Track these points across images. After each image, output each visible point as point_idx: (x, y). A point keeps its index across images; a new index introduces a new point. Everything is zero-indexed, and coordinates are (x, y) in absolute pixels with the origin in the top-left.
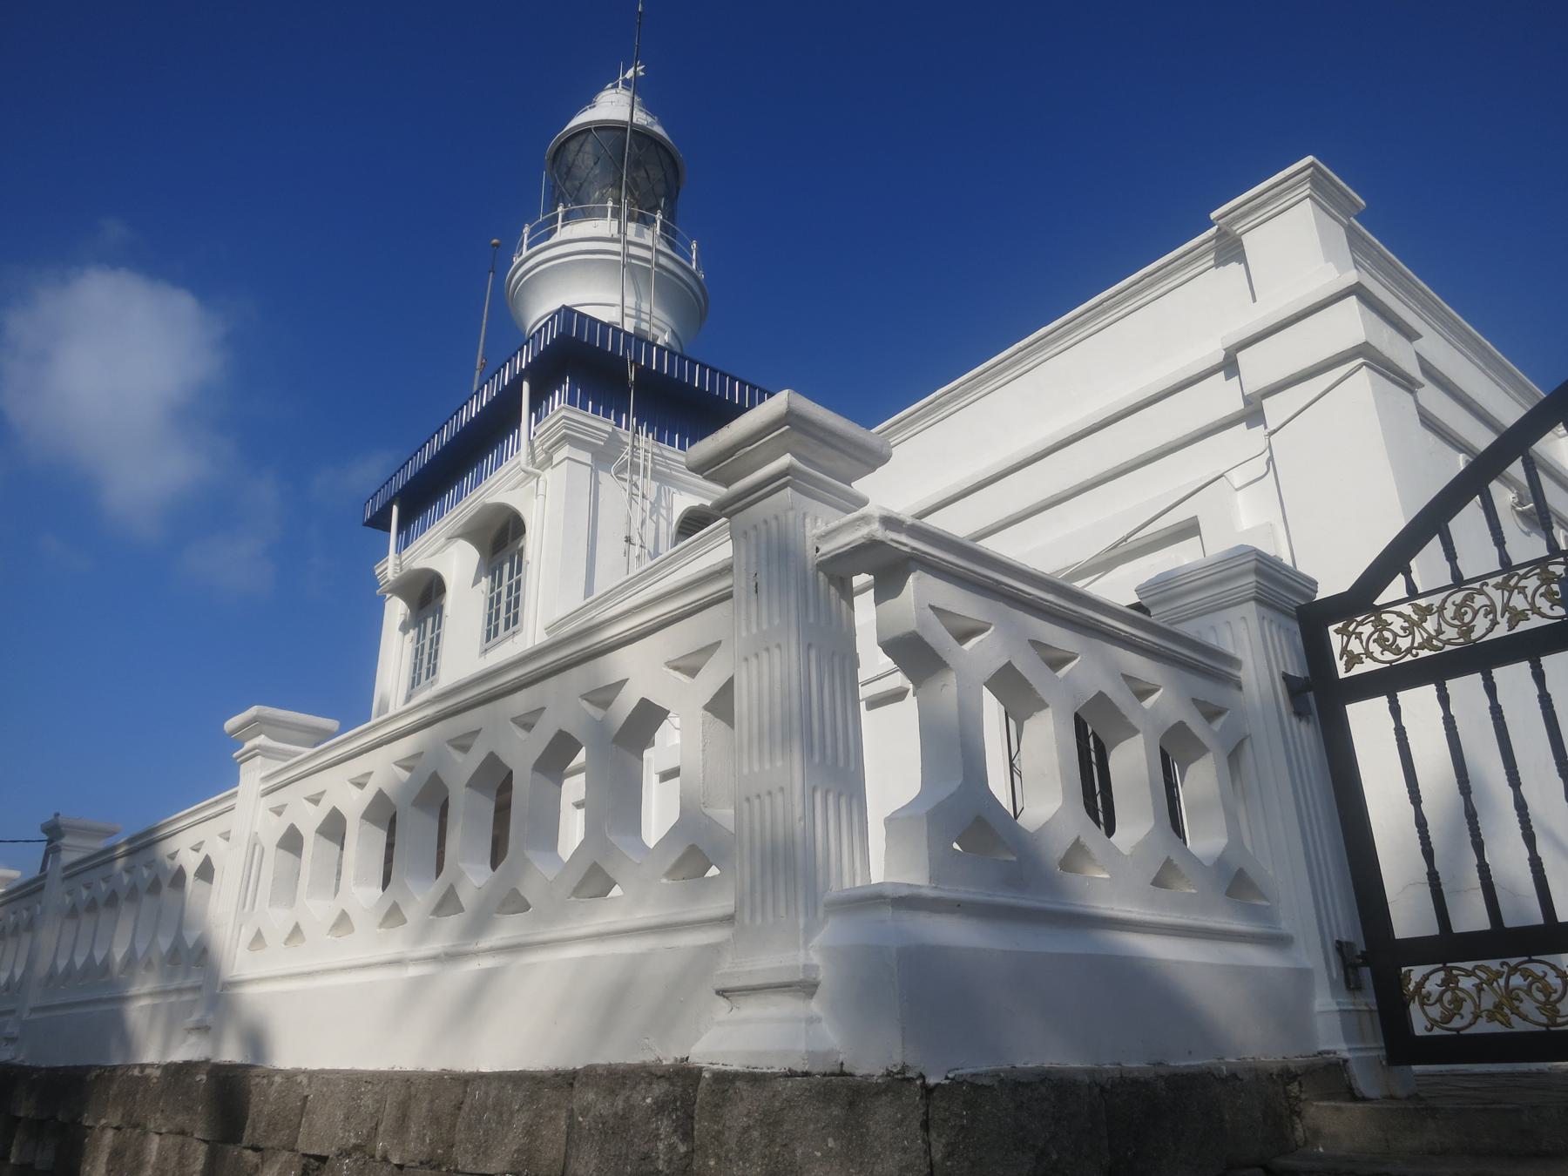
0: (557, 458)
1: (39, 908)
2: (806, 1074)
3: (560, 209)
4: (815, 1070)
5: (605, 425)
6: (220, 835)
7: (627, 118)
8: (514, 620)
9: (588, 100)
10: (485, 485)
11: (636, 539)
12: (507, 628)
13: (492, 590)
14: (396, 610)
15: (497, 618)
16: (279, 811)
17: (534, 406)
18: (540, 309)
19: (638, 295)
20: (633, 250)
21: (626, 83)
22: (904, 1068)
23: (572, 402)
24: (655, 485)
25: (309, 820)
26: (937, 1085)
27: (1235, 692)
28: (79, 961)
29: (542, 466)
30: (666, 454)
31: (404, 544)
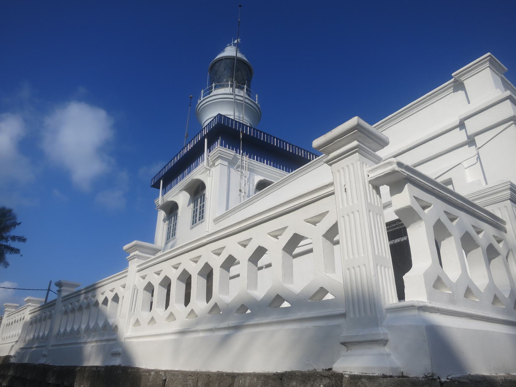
0: (216, 164)
1: (53, 312)
2: (391, 377)
3: (213, 85)
4: (394, 375)
5: (232, 153)
6: (121, 286)
7: (235, 55)
8: (202, 217)
9: (222, 50)
10: (192, 173)
11: (243, 191)
12: (199, 220)
13: (194, 208)
14: (162, 215)
15: (196, 217)
16: (144, 278)
17: (209, 147)
18: (208, 117)
19: (239, 112)
20: (237, 98)
21: (235, 45)
22: (433, 375)
23: (221, 145)
24: (248, 172)
25: (156, 280)
26: (445, 381)
27: (504, 233)
28: (69, 329)
29: (211, 167)
30: (252, 162)
31: (164, 193)
